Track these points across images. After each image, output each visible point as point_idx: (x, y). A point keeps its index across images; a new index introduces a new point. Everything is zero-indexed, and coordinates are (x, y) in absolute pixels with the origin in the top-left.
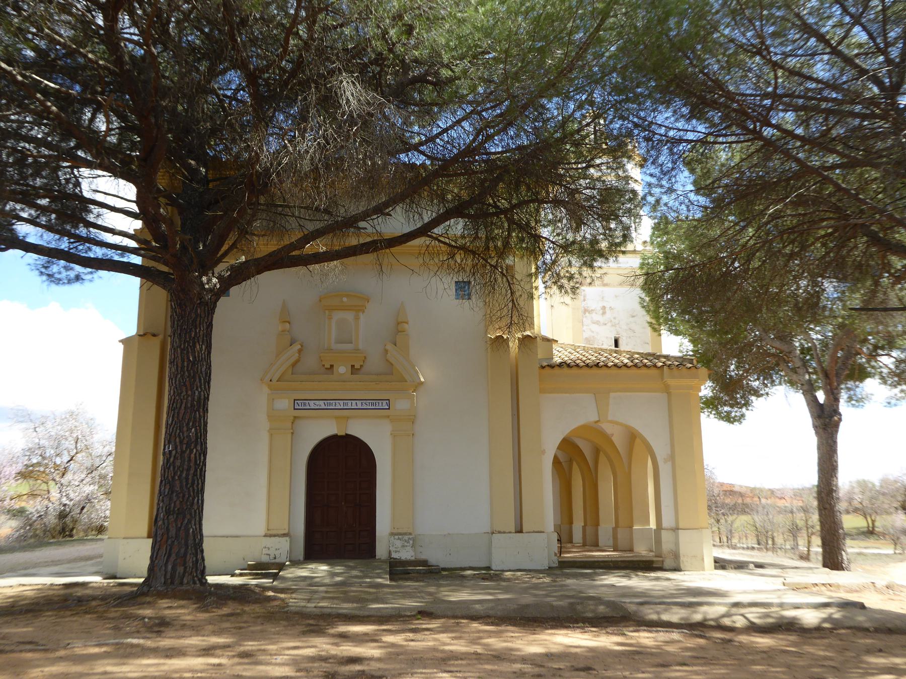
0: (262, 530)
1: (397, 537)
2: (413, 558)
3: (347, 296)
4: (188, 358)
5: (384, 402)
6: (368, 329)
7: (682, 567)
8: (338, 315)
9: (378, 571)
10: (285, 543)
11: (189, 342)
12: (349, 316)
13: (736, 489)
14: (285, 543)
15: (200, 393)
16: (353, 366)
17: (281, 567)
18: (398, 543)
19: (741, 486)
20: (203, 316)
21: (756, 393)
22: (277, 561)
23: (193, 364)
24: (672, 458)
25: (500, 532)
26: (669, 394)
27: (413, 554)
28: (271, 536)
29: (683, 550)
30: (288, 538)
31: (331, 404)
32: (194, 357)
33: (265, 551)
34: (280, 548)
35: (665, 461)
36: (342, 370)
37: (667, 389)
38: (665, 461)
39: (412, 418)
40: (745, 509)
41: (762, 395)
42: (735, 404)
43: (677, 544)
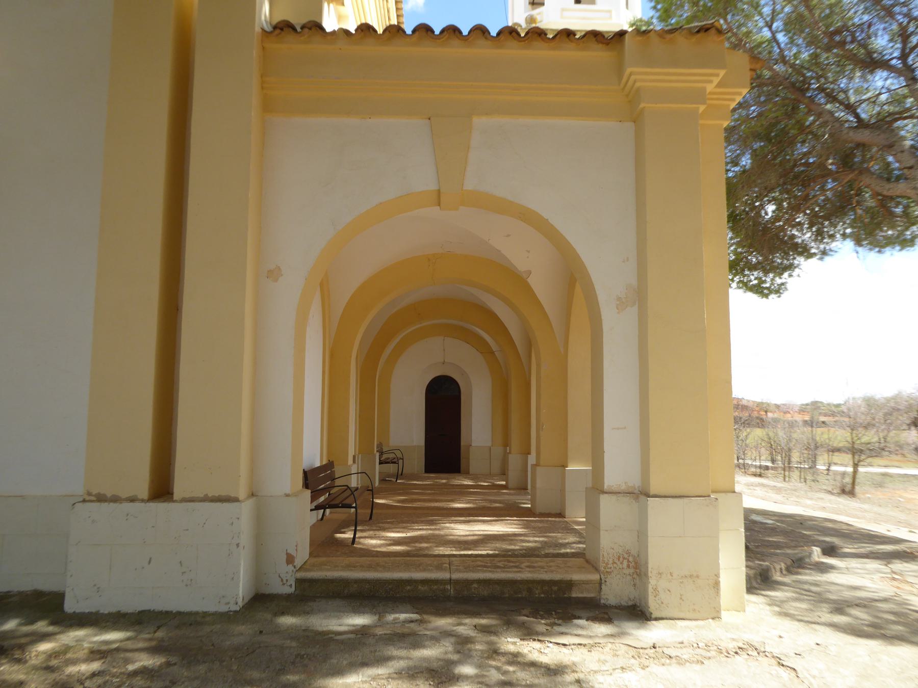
7: (653, 606)
13: (744, 403)
19: (748, 401)
21: (805, 251)
24: (639, 296)
26: (637, 118)
29: (657, 558)
35: (621, 305)
37: (632, 110)
38: (621, 305)
40: (761, 423)
41: (815, 254)
42: (768, 267)
43: (642, 535)
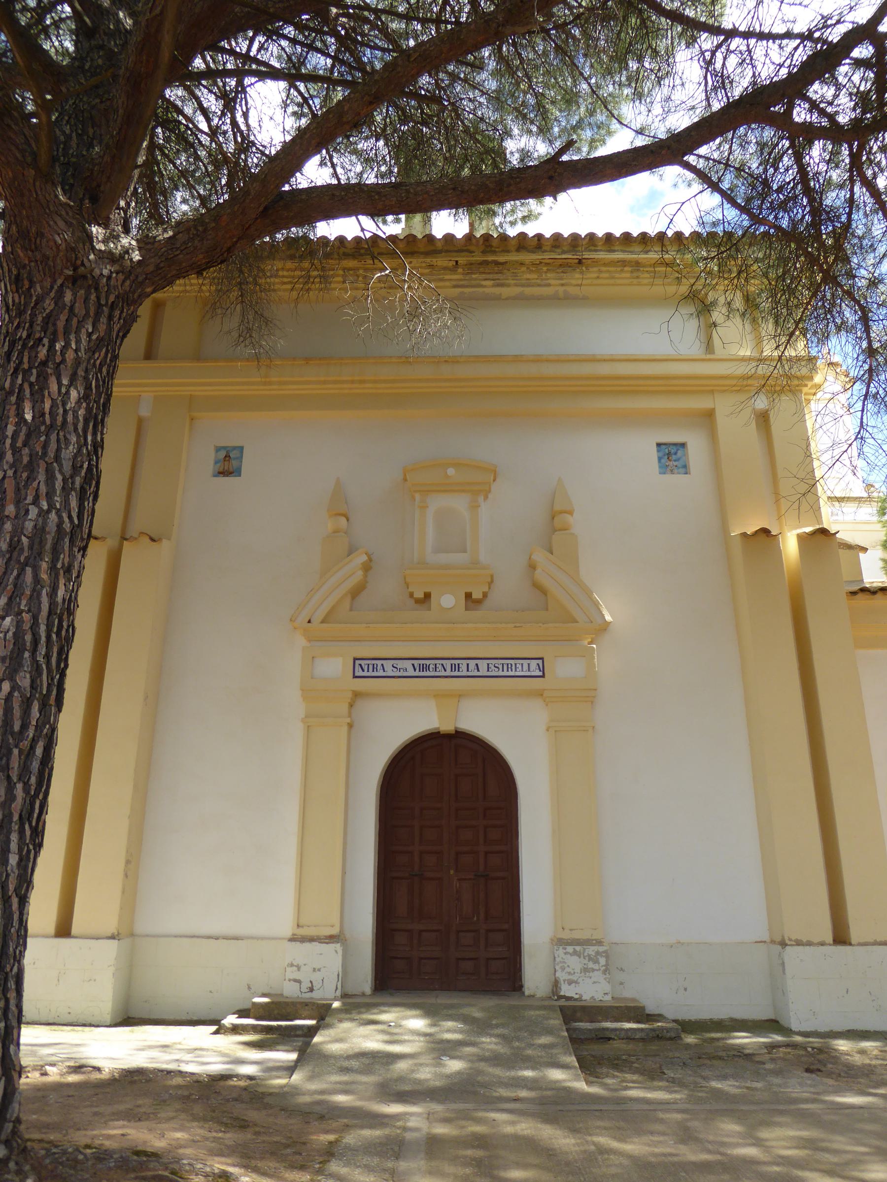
0: (288, 929)
1: (570, 949)
2: (608, 998)
3: (456, 465)
4: (20, 415)
5: (534, 663)
6: (498, 528)
8: (438, 502)
9: (544, 1040)
10: (330, 958)
11: (27, 373)
12: (459, 503)
14: (330, 958)
15: (43, 514)
16: (468, 596)
17: (323, 1014)
18: (575, 963)
20: (79, 309)
22: (316, 995)
23: (32, 432)
25: (799, 943)
27: (607, 988)
28: (303, 939)
30: (338, 946)
31: (428, 668)
32: (39, 415)
33: (292, 973)
34: (324, 970)
36: (448, 600)
39: (587, 696)
